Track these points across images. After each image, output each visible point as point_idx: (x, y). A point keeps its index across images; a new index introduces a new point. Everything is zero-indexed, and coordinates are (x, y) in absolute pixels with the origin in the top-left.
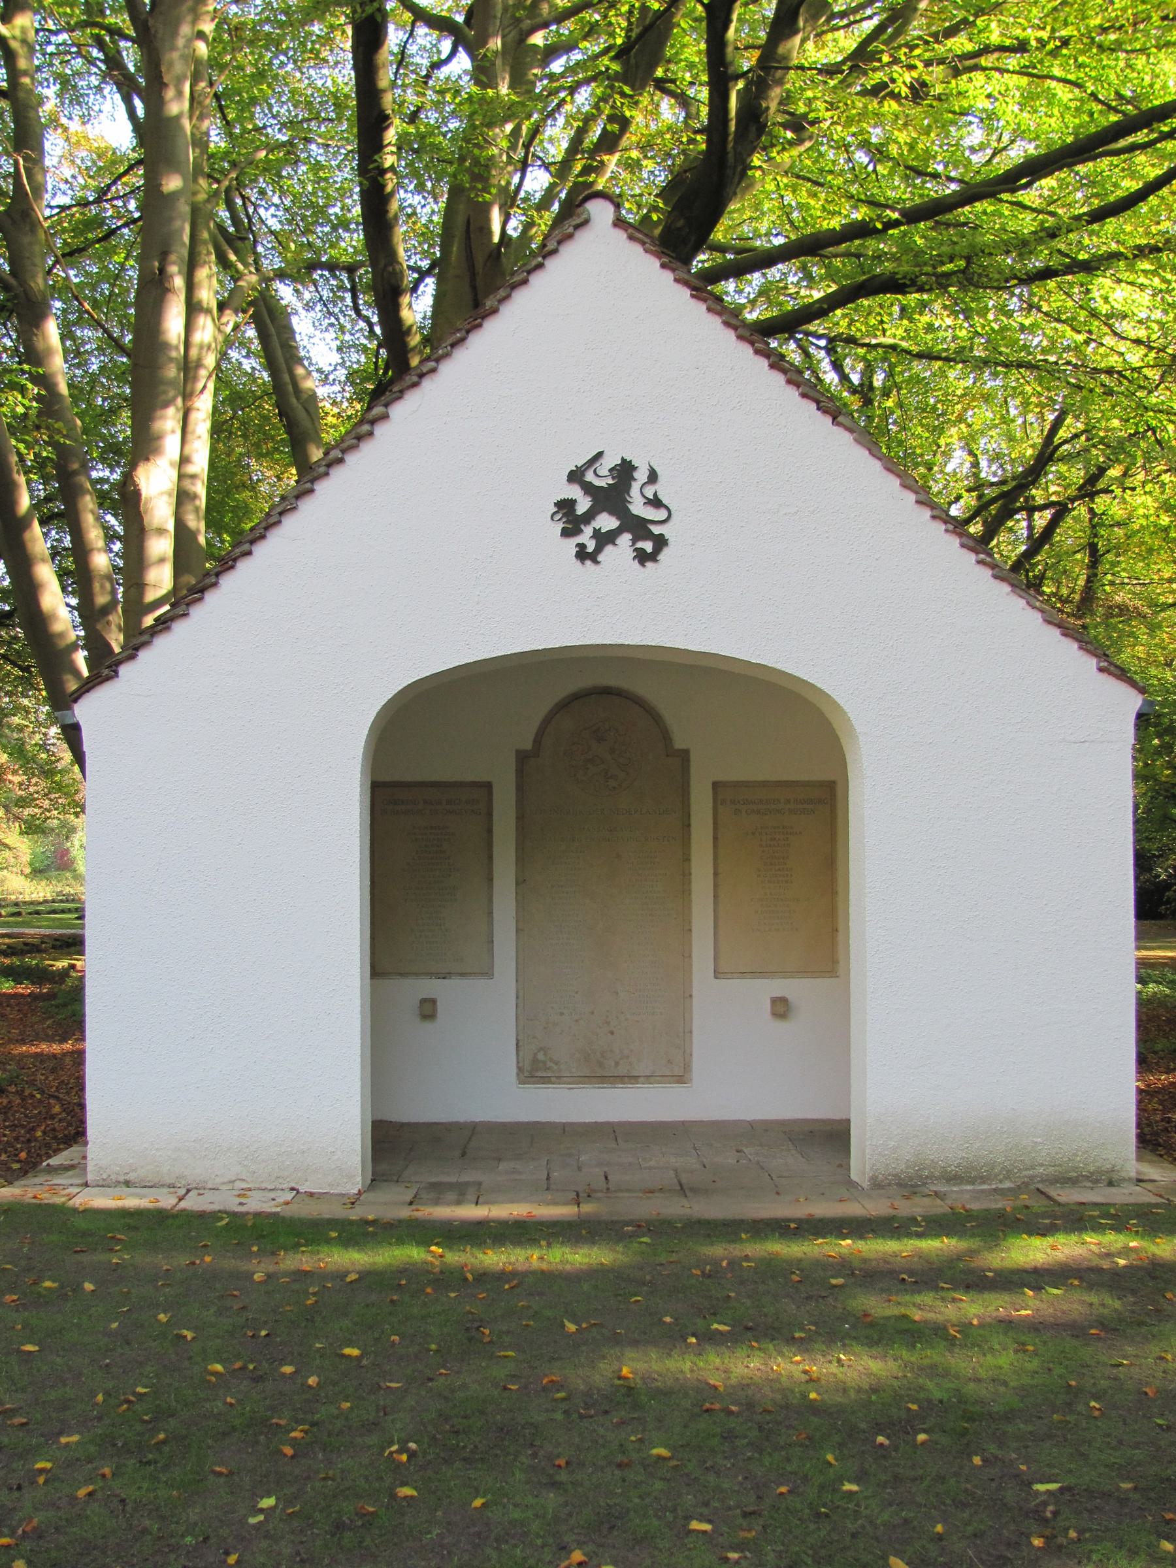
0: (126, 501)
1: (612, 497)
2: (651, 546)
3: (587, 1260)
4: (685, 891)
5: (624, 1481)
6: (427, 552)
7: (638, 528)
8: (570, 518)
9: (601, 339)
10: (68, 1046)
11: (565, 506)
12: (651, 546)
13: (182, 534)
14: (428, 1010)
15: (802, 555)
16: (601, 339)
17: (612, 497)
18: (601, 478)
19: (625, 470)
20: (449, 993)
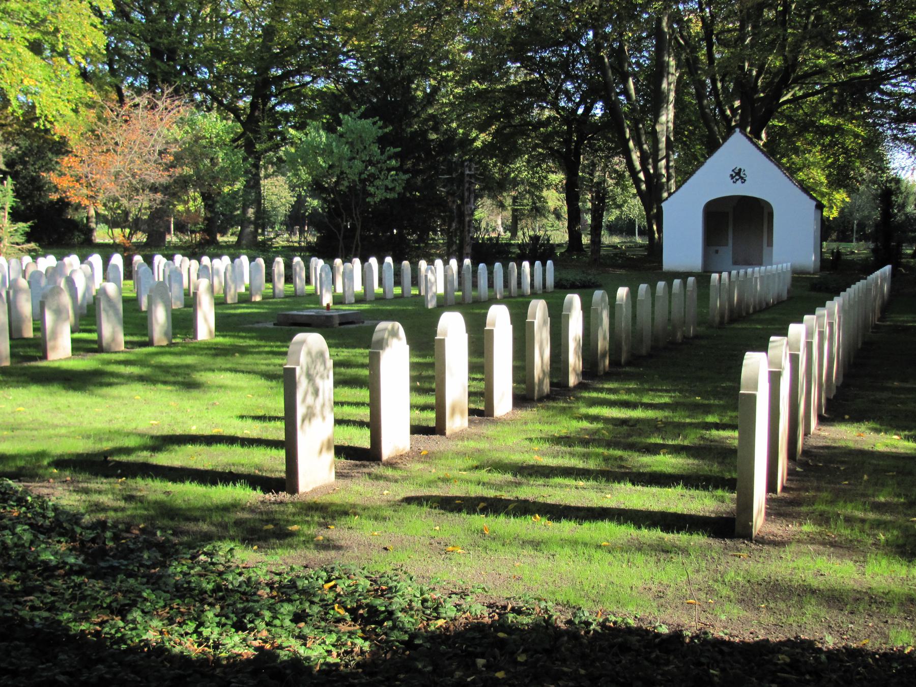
0: (654, 135)
1: (738, 174)
2: (743, 180)
3: (134, 393)
4: (762, 232)
5: (799, 595)
6: (713, 180)
7: (742, 178)
8: (732, 177)
9: (738, 150)
10: (483, 311)
11: (731, 175)
12: (743, 180)
13: (668, 138)
14: (717, 252)
15: (764, 180)
16: (738, 150)
17: (738, 174)
18: (737, 171)
19: (740, 170)
20: (720, 248)
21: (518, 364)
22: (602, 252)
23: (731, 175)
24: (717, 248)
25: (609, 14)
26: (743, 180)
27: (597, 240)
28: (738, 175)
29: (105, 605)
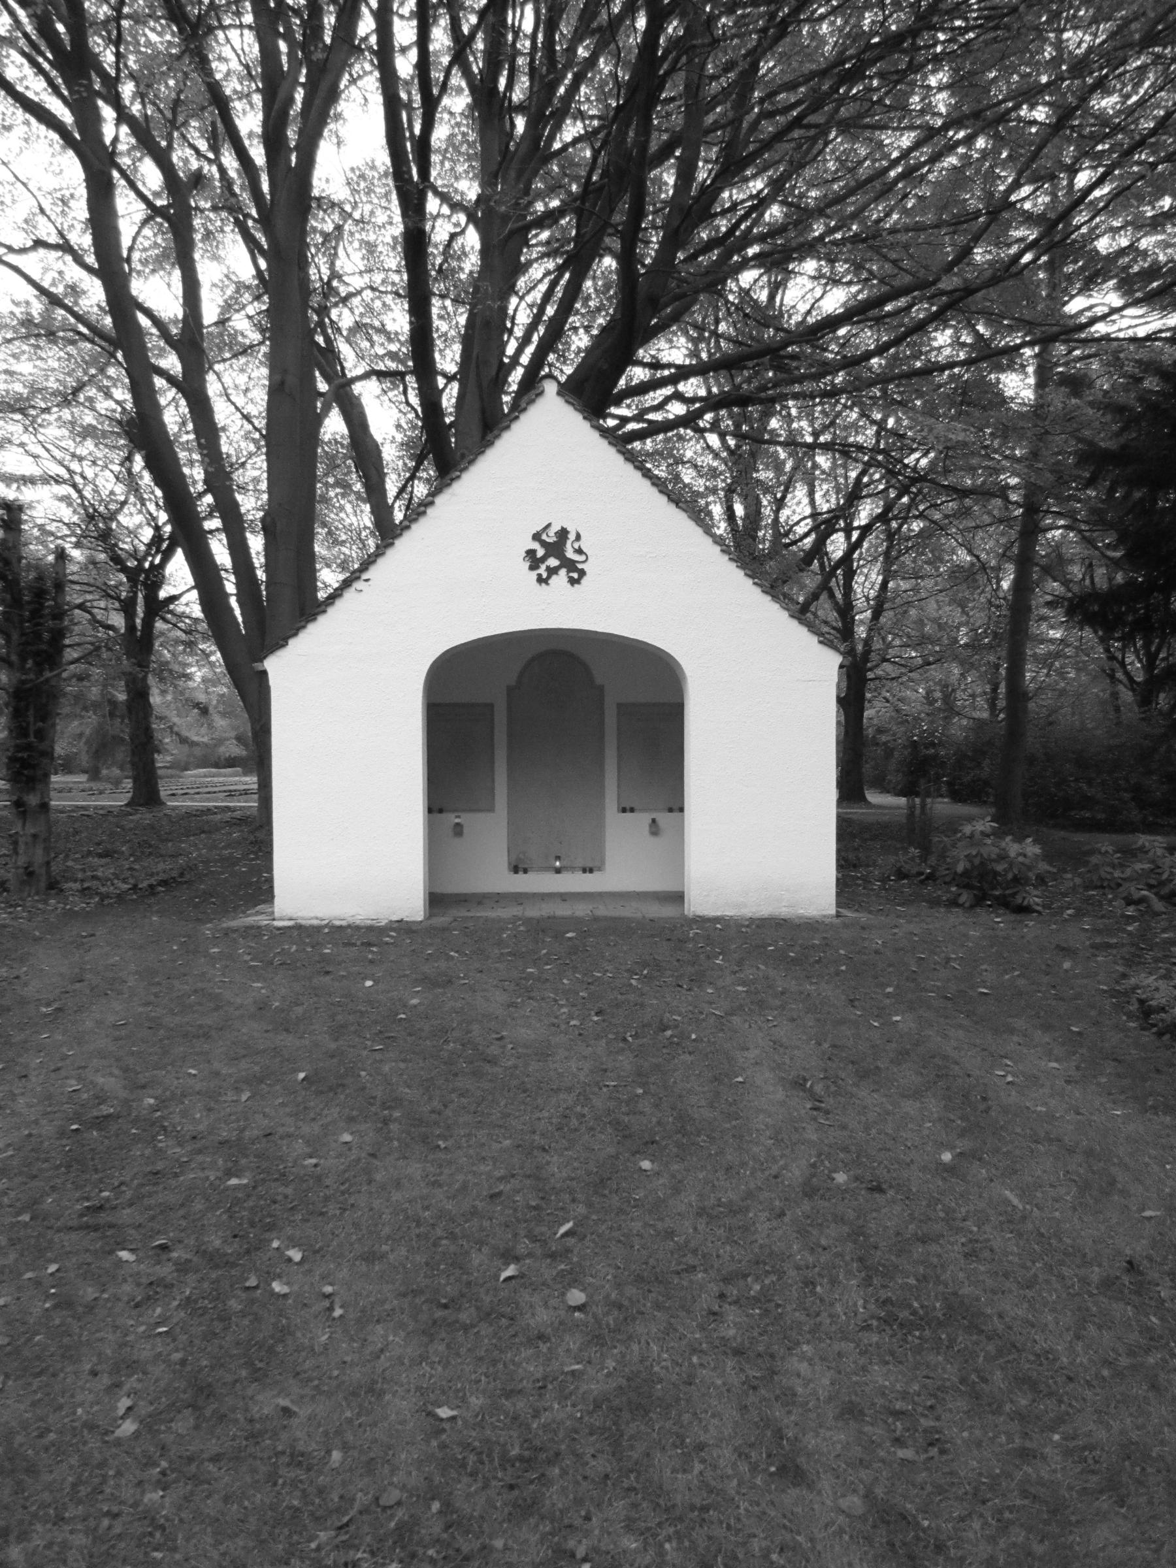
1: (556, 548)
2: (577, 575)
7: (570, 565)
8: (534, 561)
9: (548, 457)
11: (531, 553)
15: (654, 573)
16: (548, 457)
17: (556, 548)
18: (550, 538)
19: (563, 534)
21: (260, 835)
22: (1092, 468)
23: (531, 553)
24: (465, 819)
25: (104, 91)
26: (577, 575)
27: (33, 800)
28: (555, 555)
29: (795, 425)
